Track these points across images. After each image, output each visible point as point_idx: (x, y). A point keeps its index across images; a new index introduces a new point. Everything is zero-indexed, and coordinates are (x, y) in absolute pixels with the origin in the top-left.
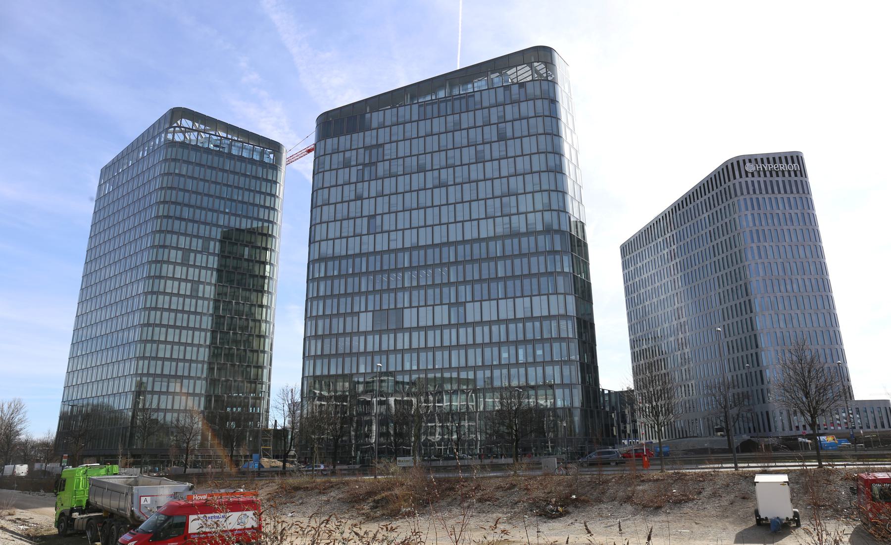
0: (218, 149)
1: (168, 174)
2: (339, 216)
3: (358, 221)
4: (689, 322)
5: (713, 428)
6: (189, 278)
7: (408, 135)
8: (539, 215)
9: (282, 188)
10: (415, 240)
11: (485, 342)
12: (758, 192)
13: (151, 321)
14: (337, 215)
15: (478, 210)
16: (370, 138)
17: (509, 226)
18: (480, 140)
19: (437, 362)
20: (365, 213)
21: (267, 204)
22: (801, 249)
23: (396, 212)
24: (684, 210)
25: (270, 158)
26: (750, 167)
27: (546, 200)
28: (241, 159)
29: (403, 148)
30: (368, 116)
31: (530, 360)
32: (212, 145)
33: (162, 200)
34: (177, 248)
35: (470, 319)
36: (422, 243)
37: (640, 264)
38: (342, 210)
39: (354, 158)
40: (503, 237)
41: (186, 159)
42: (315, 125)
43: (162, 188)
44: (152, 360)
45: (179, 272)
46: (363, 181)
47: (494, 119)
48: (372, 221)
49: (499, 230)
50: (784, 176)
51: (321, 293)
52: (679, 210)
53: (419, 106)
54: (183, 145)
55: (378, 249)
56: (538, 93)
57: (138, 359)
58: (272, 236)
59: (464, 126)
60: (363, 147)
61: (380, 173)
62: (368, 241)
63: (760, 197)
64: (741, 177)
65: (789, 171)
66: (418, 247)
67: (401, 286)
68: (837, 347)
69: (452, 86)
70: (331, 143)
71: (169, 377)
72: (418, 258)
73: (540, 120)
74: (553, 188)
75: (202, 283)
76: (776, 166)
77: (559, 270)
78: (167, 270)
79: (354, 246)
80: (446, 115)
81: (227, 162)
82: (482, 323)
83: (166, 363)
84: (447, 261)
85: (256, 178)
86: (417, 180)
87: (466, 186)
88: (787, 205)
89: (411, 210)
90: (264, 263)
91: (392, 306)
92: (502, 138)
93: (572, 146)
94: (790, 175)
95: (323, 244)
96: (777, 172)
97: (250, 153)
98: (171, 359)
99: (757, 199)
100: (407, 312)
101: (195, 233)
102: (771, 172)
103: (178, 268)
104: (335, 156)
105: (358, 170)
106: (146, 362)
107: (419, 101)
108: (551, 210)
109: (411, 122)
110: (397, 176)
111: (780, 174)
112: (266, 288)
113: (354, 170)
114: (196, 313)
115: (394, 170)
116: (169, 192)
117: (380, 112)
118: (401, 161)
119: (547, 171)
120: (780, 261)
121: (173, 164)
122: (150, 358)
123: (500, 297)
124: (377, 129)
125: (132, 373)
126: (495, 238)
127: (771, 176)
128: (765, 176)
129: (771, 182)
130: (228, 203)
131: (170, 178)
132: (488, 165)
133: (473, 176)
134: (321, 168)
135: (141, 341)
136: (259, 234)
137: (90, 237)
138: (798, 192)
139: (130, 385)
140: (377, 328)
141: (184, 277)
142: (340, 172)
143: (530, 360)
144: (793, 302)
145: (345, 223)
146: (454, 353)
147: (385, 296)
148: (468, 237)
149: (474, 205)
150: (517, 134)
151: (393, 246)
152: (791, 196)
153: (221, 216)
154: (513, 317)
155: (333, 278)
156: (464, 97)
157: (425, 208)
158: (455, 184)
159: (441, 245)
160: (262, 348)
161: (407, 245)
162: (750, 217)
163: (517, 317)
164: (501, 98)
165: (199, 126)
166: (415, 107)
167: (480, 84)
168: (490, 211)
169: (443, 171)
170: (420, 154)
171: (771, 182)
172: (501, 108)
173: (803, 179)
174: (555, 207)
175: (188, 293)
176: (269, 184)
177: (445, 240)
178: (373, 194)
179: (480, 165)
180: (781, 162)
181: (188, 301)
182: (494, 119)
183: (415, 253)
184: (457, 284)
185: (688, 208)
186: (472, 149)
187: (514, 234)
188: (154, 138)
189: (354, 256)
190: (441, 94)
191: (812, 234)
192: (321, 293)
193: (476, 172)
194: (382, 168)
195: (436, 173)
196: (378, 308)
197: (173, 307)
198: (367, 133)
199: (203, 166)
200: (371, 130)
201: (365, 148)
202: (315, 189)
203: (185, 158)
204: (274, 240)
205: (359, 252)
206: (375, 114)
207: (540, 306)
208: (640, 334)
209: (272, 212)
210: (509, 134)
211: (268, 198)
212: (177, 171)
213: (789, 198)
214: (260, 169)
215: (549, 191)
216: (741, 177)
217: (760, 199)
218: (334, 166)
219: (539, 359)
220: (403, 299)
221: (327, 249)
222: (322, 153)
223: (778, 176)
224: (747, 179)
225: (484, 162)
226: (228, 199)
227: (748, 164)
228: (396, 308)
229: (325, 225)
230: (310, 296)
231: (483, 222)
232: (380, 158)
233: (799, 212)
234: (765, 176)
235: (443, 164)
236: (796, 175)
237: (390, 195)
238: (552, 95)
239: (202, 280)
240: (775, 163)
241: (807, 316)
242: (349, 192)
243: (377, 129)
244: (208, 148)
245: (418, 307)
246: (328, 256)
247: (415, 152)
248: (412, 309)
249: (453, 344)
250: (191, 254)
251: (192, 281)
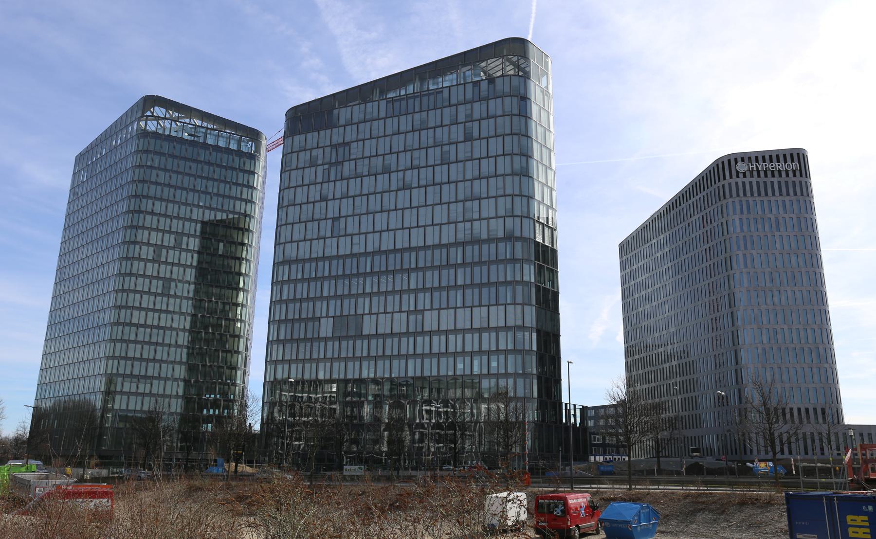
0: (192, 138)
1: (140, 166)
2: (304, 218)
3: (323, 223)
4: (678, 332)
5: (689, 448)
6: (160, 276)
7: (375, 133)
8: (501, 221)
9: (260, 179)
10: (377, 245)
11: (474, 350)
12: (749, 194)
13: (122, 320)
14: (302, 217)
15: (440, 214)
16: (337, 136)
17: (470, 232)
18: (446, 140)
19: (393, 371)
20: (330, 215)
21: (244, 197)
22: (793, 258)
23: (360, 215)
24: (677, 210)
25: (247, 146)
26: (742, 167)
27: (509, 206)
28: (217, 148)
29: (370, 148)
30: (336, 112)
31: (485, 371)
32: (186, 134)
33: (133, 194)
34: (148, 244)
35: (427, 328)
36: (384, 248)
37: (635, 267)
38: (307, 210)
39: (320, 157)
40: (464, 244)
41: (158, 151)
42: (284, 119)
43: (133, 181)
44: (121, 359)
45: (151, 269)
46: (329, 181)
47: (461, 118)
48: (336, 223)
49: (461, 236)
50: (780, 176)
51: (285, 297)
52: (673, 210)
53: (387, 102)
54: (155, 135)
55: (341, 253)
56: (507, 89)
57: (108, 358)
58: (248, 230)
59: (431, 124)
60: (330, 145)
61: (346, 173)
62: (331, 243)
63: (751, 200)
64: (731, 177)
65: (787, 172)
66: (380, 252)
67: (362, 292)
68: (826, 365)
69: (422, 80)
70: (299, 140)
71: (139, 377)
72: (379, 263)
73: (508, 119)
74: (517, 192)
75: (174, 280)
76: (772, 165)
77: (518, 278)
78: (138, 267)
79: (317, 249)
80: (414, 113)
81: (202, 152)
82: (439, 332)
83: (136, 363)
84: (408, 267)
85: (233, 169)
86: (382, 181)
87: (430, 189)
88: (781, 209)
89: (374, 213)
90: (241, 259)
91: (352, 312)
92: (468, 138)
93: (543, 146)
94: (787, 175)
95: (288, 246)
96: (773, 172)
97: (226, 142)
98: (141, 359)
99: (748, 202)
100: (366, 318)
101: (167, 229)
102: (765, 172)
103: (150, 265)
104: (302, 154)
105: (324, 170)
106: (116, 362)
107: (388, 97)
108: (513, 216)
109: (379, 119)
110: (362, 177)
111: (776, 174)
112: (241, 286)
113: (320, 169)
114: (167, 312)
115: (359, 170)
116: (140, 185)
117: (348, 108)
118: (366, 161)
119: (512, 174)
120: (768, 270)
121: (145, 156)
122: (120, 358)
123: (458, 306)
124: (345, 126)
125: (101, 373)
126: (456, 244)
127: (766, 176)
128: (759, 176)
129: (765, 183)
130: (203, 196)
131: (142, 170)
132: (453, 167)
133: (438, 179)
134: (288, 167)
135: (111, 340)
136: (235, 228)
137: (65, 229)
138: (795, 194)
139: (100, 384)
140: (337, 334)
141: (155, 274)
142: (307, 171)
143: (485, 371)
144: (780, 316)
145: (309, 224)
146: (411, 362)
147: (346, 302)
148: (429, 242)
149: (437, 208)
150: (484, 134)
151: (355, 250)
152: (787, 199)
153: (195, 210)
154: (470, 327)
155: (296, 281)
156: (433, 93)
157: (388, 211)
158: (419, 187)
159: (402, 250)
160: (236, 349)
161: (370, 249)
162: (737, 222)
164: (469, 95)
165: (173, 113)
166: (383, 103)
167: (450, 80)
168: (453, 216)
169: (408, 173)
170: (386, 154)
171: (765, 183)
172: (469, 106)
173: (803, 179)
174: (517, 212)
175: (160, 291)
176: (246, 175)
177: (406, 245)
178: (338, 195)
179: (445, 167)
180: (778, 161)
181: (159, 299)
182: (461, 118)
183: (377, 258)
184: (416, 291)
185: (681, 208)
186: (438, 149)
187: (475, 241)
188: (127, 127)
189: (317, 259)
190: (410, 89)
191: (808, 241)
192: (285, 297)
193: (441, 174)
194: (348, 168)
195: (401, 174)
196: (338, 313)
197: (144, 305)
198: (335, 130)
199: (176, 157)
200: (338, 127)
201: (331, 146)
202: (282, 188)
203: (157, 149)
204: (251, 234)
205: (322, 255)
206: (343, 110)
207: (497, 317)
208: (633, 342)
209: (249, 205)
210: (476, 134)
211: (245, 190)
212: (149, 164)
213: (784, 201)
214: (237, 159)
215: (513, 195)
216: (731, 177)
217: (751, 202)
218: (301, 165)
219: (493, 371)
220: (364, 305)
221: (291, 251)
222: (290, 151)
223: (773, 176)
224: (738, 180)
225: (449, 163)
226: (203, 192)
227: (740, 163)
228: (356, 314)
229: (290, 227)
230: (274, 300)
231: (445, 228)
232: (347, 158)
233: (794, 216)
234: (759, 176)
235: (409, 164)
236: (795, 175)
237: (354, 197)
238: (522, 91)
239: (174, 277)
240: (771, 161)
241: (794, 331)
242: (315, 193)
243: (345, 126)
244: (182, 139)
245: (377, 314)
246: (292, 259)
247: (381, 152)
248: (372, 316)
249: (425, 352)
250: (184, 237)
251: (164, 279)
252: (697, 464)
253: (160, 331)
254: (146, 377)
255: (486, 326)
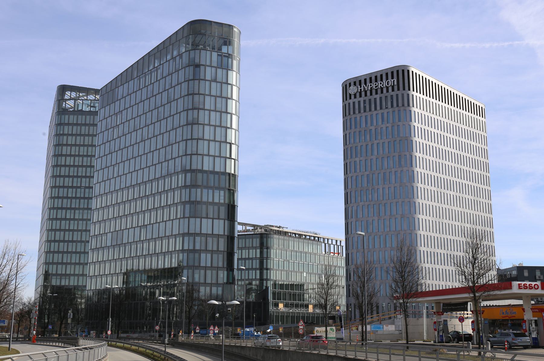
71: (61, 275)
76: (376, 84)
163: (202, 232)
252: (7, 333)
253: (73, 243)
254: (66, 275)
255: (211, 233)
